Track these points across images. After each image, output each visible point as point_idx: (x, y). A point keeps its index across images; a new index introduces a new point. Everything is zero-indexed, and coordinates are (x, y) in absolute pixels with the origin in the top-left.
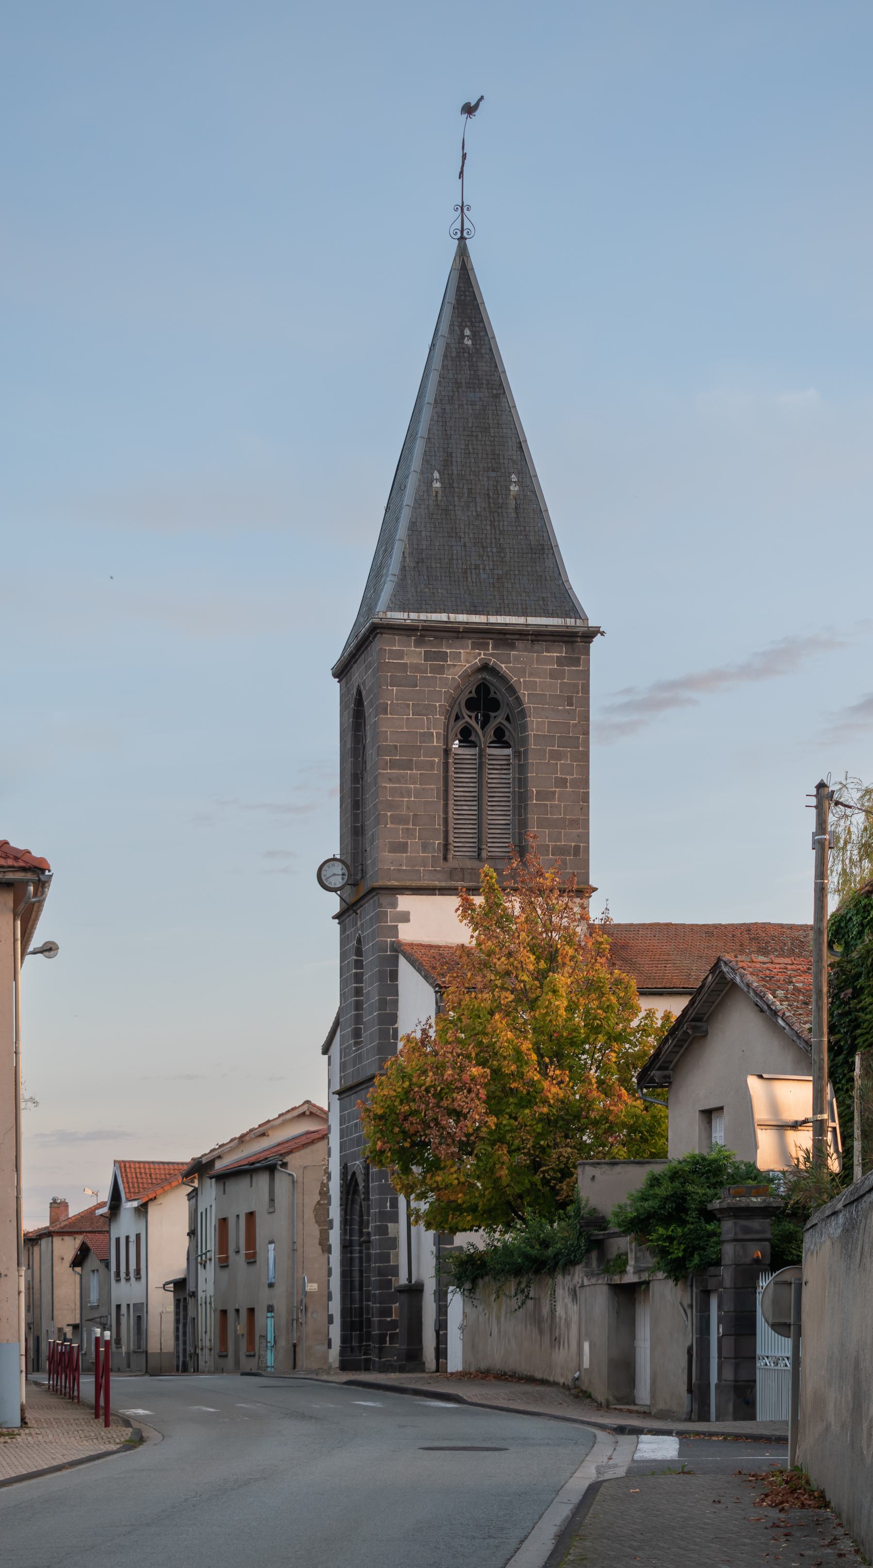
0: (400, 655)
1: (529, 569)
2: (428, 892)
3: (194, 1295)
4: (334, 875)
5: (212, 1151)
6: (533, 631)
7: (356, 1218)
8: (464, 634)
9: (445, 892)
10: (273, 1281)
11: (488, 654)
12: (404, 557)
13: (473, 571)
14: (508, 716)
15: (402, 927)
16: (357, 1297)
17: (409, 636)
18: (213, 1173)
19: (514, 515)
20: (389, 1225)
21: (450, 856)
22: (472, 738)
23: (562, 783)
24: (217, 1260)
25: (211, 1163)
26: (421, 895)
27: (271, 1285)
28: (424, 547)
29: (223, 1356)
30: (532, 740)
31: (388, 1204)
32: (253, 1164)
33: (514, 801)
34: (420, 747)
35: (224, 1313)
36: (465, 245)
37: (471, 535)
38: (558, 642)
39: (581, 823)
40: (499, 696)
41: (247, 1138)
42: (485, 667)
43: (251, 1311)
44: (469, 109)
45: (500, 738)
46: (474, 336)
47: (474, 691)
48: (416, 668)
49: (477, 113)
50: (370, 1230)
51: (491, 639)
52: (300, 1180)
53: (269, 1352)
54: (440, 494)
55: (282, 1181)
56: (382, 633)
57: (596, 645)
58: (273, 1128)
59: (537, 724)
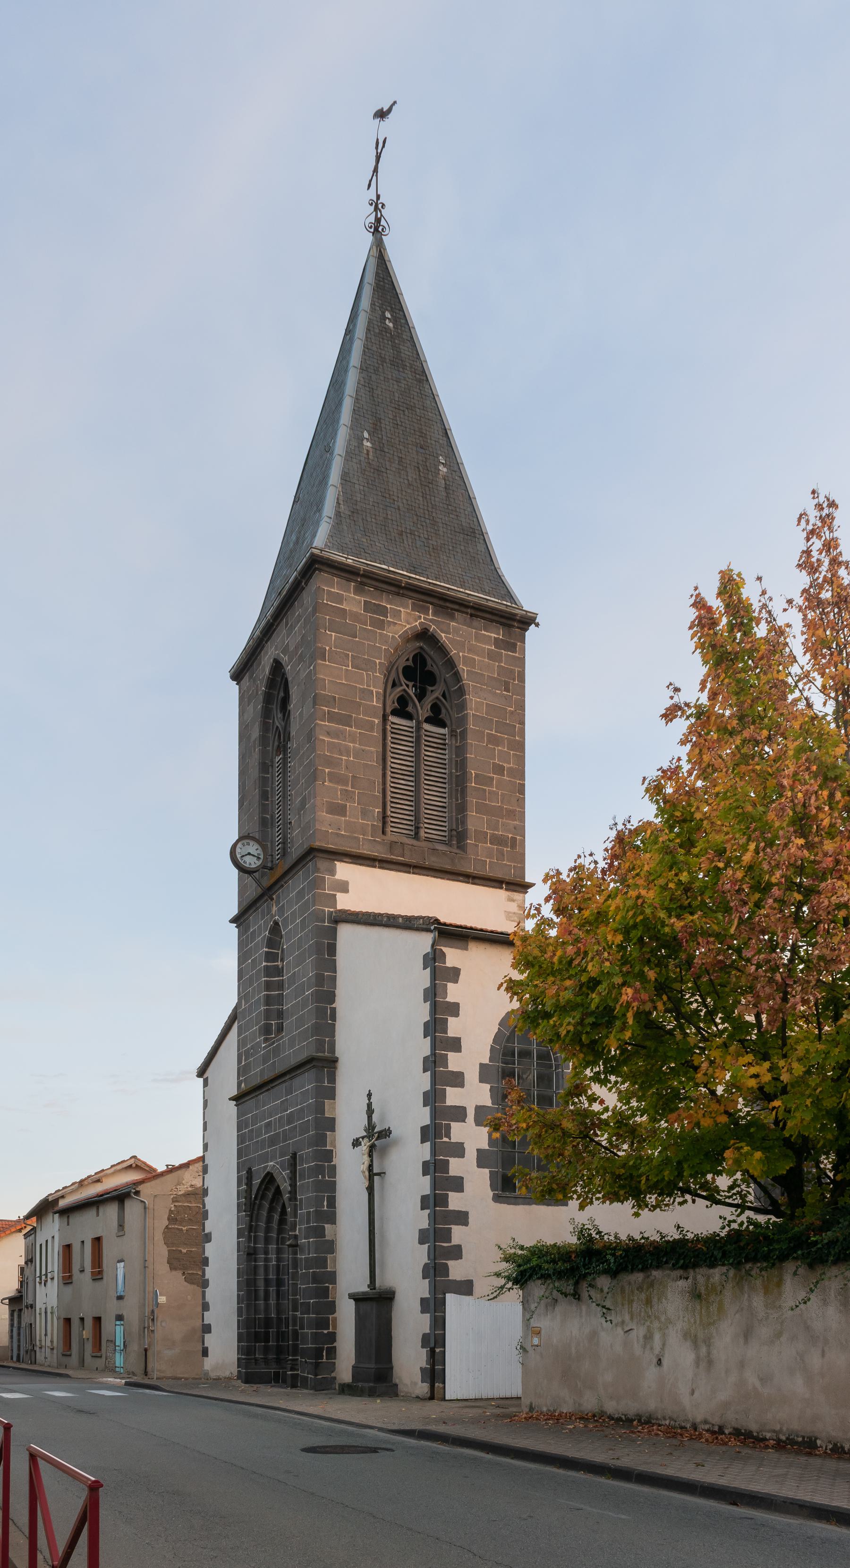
0: (339, 599)
1: (463, 548)
2: (368, 862)
3: (32, 1306)
4: (249, 854)
5: (57, 1191)
6: (475, 603)
7: (262, 1224)
8: (406, 592)
9: (385, 865)
10: (122, 1294)
11: (427, 619)
12: (338, 503)
13: (409, 535)
14: (444, 693)
15: (340, 896)
16: (262, 1307)
17: (349, 580)
18: (56, 1209)
19: (444, 494)
20: (326, 1226)
21: (389, 829)
22: (410, 709)
23: (499, 770)
24: (61, 1279)
25: (56, 1201)
26: (360, 865)
27: (120, 1298)
28: (359, 499)
29: (66, 1354)
30: (471, 720)
31: (325, 1203)
32: (102, 1195)
33: (450, 783)
34: (359, 704)
35: (68, 1321)
36: (381, 240)
37: (405, 501)
38: (497, 622)
39: (518, 814)
40: (435, 670)
41: (86, 1183)
42: (424, 635)
43: (98, 1320)
44: (381, 114)
45: (436, 719)
46: (395, 320)
47: (411, 659)
48: (356, 617)
49: (390, 116)
50: (297, 1233)
51: (431, 603)
52: (151, 1206)
53: (118, 1355)
54: (371, 454)
55: (132, 1208)
56: (320, 570)
57: (531, 633)
58: (106, 1176)
59: (477, 703)
